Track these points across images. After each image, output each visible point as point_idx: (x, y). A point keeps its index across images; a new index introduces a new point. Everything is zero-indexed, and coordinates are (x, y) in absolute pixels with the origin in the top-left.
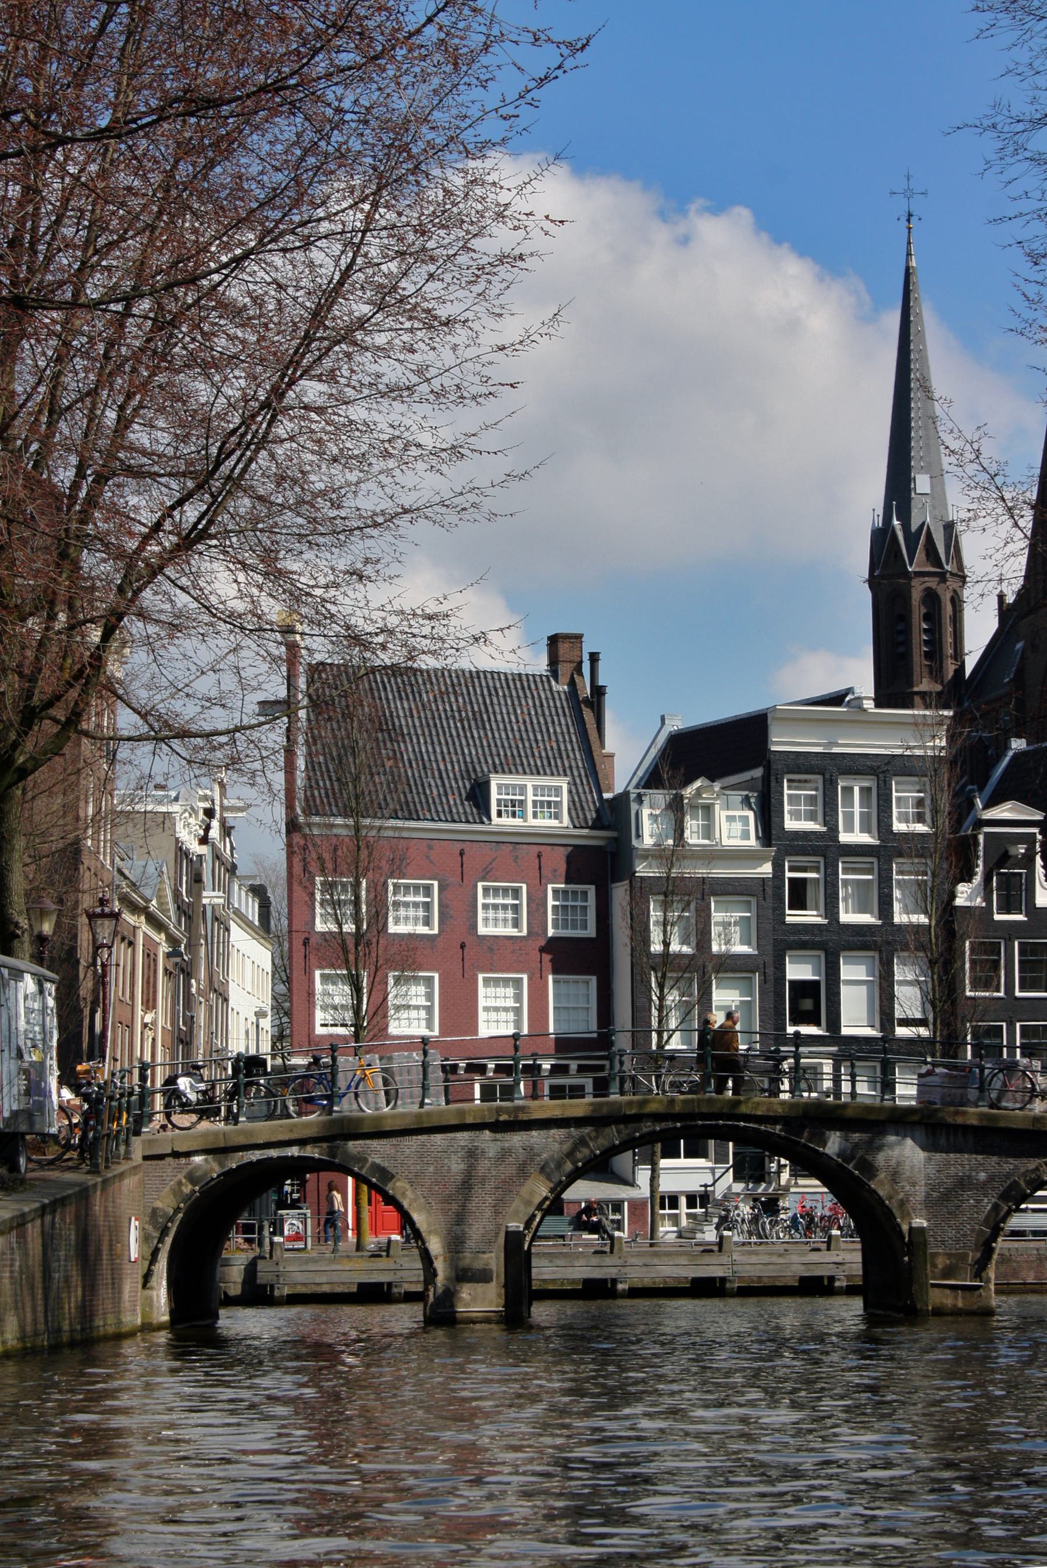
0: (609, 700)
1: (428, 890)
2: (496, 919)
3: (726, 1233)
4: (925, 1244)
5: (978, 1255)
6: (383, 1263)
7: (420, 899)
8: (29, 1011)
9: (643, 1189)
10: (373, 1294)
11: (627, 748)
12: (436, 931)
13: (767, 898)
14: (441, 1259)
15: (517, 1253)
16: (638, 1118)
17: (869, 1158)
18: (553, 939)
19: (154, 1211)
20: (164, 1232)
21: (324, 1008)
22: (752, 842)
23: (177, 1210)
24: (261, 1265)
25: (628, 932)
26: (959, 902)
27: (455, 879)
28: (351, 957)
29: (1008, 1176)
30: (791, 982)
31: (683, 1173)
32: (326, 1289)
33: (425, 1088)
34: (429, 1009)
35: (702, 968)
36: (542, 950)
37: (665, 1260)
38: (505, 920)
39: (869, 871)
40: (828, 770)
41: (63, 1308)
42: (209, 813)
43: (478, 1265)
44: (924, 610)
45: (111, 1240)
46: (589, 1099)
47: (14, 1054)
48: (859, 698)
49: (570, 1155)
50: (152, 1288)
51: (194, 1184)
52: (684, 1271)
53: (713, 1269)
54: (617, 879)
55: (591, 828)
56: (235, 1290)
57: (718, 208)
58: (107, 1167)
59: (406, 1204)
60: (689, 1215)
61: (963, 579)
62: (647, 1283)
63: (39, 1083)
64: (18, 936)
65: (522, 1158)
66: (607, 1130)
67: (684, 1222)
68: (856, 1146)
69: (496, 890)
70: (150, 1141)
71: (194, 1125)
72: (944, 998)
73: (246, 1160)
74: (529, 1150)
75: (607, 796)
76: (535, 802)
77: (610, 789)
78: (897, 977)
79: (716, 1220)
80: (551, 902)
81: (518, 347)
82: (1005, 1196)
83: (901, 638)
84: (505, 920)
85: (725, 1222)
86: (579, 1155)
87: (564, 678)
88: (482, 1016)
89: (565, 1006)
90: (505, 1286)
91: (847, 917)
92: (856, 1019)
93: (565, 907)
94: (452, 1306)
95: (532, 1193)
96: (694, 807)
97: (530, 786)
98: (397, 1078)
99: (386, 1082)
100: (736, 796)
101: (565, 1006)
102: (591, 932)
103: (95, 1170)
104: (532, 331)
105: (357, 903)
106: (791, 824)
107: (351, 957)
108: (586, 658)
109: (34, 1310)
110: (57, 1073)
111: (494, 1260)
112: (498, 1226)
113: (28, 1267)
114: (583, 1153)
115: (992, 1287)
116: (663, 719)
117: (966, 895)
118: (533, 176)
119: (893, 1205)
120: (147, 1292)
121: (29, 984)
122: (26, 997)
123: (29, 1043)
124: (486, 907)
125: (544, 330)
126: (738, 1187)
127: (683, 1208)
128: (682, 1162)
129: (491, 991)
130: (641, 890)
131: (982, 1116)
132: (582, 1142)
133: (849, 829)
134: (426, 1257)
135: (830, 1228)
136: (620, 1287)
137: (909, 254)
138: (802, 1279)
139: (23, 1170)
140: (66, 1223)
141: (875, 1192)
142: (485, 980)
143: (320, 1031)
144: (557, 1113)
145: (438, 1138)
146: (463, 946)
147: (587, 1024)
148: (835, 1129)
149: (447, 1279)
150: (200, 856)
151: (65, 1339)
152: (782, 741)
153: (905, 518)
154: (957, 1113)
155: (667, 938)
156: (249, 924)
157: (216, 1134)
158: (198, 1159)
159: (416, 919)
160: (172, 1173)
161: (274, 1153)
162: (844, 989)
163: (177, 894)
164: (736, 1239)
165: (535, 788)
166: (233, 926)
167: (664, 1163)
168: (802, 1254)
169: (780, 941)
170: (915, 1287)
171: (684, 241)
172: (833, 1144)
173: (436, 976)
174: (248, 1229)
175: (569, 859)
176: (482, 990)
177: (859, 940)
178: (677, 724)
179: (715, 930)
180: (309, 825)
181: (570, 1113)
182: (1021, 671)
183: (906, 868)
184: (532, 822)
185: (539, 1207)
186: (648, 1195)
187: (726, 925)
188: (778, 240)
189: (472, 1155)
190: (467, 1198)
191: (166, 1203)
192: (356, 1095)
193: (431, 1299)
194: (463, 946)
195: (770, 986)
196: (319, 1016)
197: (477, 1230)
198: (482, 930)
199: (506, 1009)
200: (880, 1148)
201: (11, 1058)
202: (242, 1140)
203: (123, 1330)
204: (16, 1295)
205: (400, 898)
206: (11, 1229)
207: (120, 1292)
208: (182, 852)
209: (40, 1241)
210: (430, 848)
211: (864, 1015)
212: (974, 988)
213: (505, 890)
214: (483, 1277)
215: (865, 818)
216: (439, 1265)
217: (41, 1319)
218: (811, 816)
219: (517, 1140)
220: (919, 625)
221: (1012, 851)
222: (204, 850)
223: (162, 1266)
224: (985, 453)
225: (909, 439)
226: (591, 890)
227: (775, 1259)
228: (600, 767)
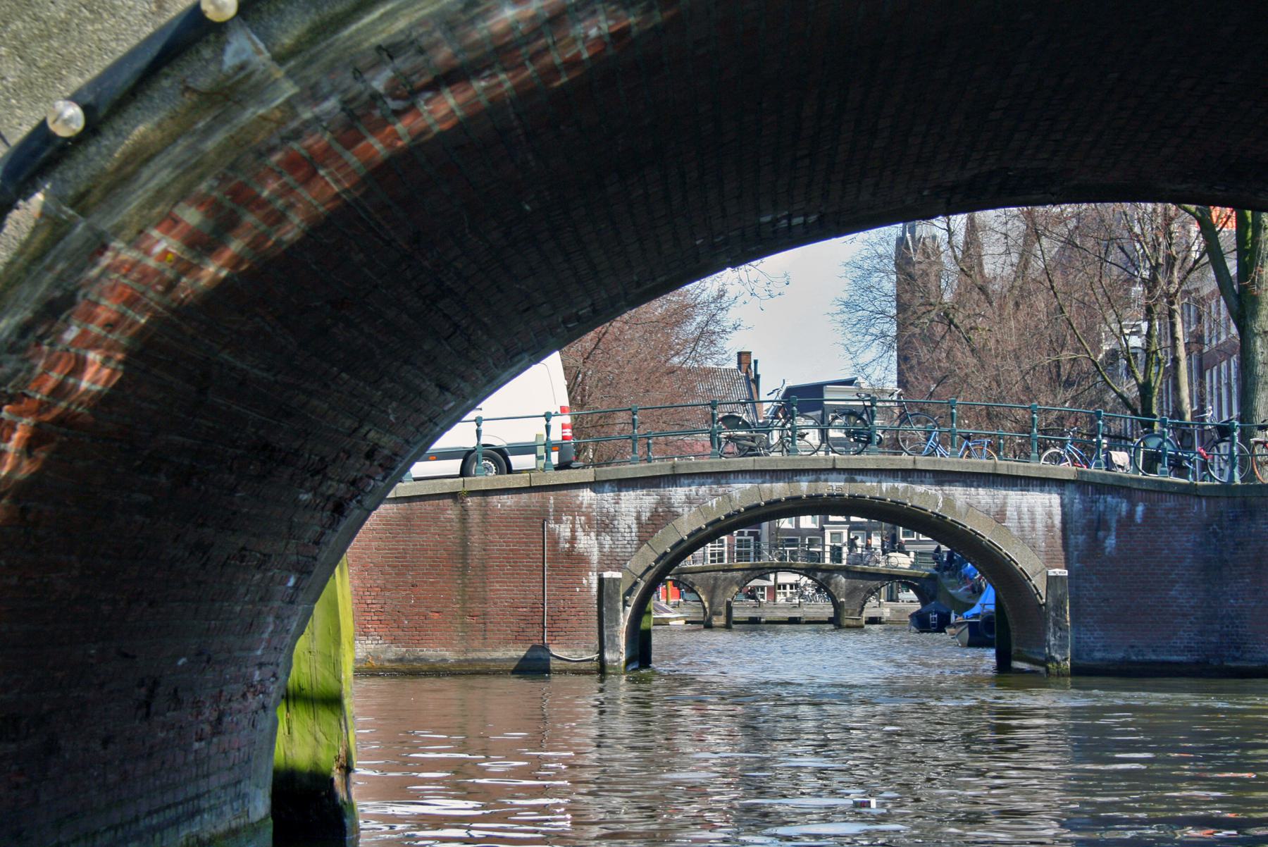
0: (761, 380)
9: (772, 583)
53: (796, 614)
111: (723, 609)
178: (790, 383)
214: (720, 614)
219: (729, 574)
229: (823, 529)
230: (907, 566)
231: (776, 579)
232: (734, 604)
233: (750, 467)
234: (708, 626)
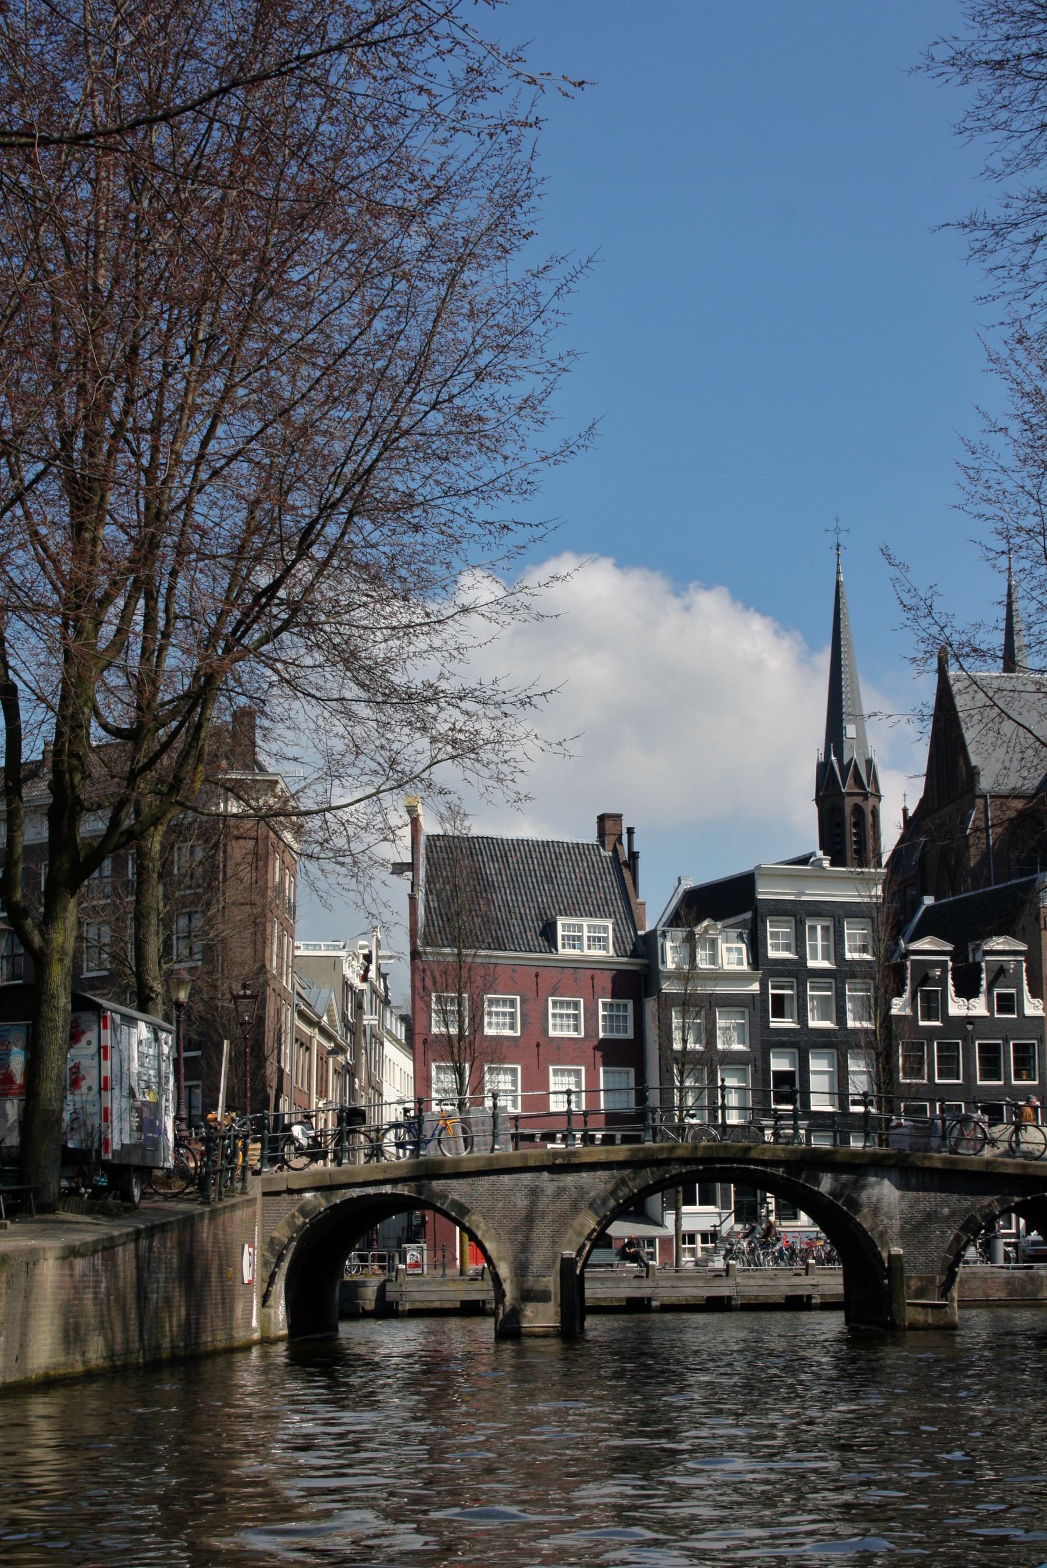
0: (641, 863)
1: (513, 1003)
2: (562, 1025)
3: (731, 1262)
4: (902, 1268)
5: (944, 1278)
7: (508, 1010)
8: (142, 1056)
9: (670, 1229)
11: (656, 899)
12: (519, 1034)
14: (509, 1281)
15: (572, 1279)
16: (667, 1162)
17: (854, 1196)
18: (603, 1040)
19: (272, 1239)
20: (280, 1258)
22: (745, 967)
23: (291, 1239)
24: (389, 1287)
25: (657, 1031)
26: (894, 1011)
27: (531, 995)
28: (456, 1050)
29: (966, 1211)
30: (775, 1072)
31: (699, 1217)
32: (437, 1305)
33: (495, 1136)
36: (595, 1048)
37: (687, 1283)
38: (568, 1026)
40: (799, 913)
41: (163, 1327)
42: (368, 958)
43: (540, 1287)
45: (221, 1265)
47: (125, 1093)
49: (613, 1193)
50: (270, 1307)
51: (305, 1217)
53: (723, 1289)
54: (648, 995)
55: (630, 957)
56: (370, 1305)
57: (708, 588)
58: (220, 1199)
59: (479, 1234)
60: (703, 1249)
61: (879, 797)
62: (674, 1300)
63: (153, 1122)
64: (152, 999)
65: (574, 1195)
66: (643, 1172)
67: (699, 1254)
68: (844, 1186)
69: (562, 1003)
70: (269, 1180)
71: (306, 1166)
73: (348, 1196)
74: (580, 1188)
75: (640, 933)
76: (589, 938)
77: (643, 928)
78: (850, 1069)
79: (723, 1252)
81: (558, 457)
82: (964, 1228)
83: (838, 839)
84: (568, 1026)
85: (729, 1254)
86: (620, 1194)
90: (561, 1305)
93: (611, 1016)
94: (518, 1322)
95: (583, 1225)
98: (474, 1129)
99: (464, 1131)
100: (733, 933)
102: (630, 1035)
103: (206, 1202)
104: (571, 442)
105: (460, 1013)
106: (772, 954)
107: (456, 1050)
108: (624, 831)
109: (126, 1329)
110: (172, 1114)
111: (551, 1282)
112: (555, 1254)
113: (117, 1289)
114: (624, 1192)
115: (956, 1305)
116: (679, 880)
117: (899, 1006)
118: (569, 278)
119: (874, 1235)
120: (266, 1310)
121: (142, 1031)
122: (140, 1043)
123: (143, 1085)
124: (554, 1015)
125: (581, 442)
126: (738, 1228)
127: (699, 1243)
128: (697, 1208)
129: (559, 1079)
130: (666, 1003)
131: (945, 1160)
132: (623, 1182)
133: (814, 957)
135: (807, 1258)
136: (654, 1303)
137: (838, 572)
138: (788, 1297)
139: (137, 1199)
140: (167, 1250)
141: (860, 1224)
144: (602, 1158)
145: (506, 1179)
146: (538, 1045)
147: (627, 1103)
148: (826, 1171)
149: (514, 1299)
150: (362, 991)
151: (164, 1356)
152: (765, 892)
153: (839, 755)
154: (924, 1158)
157: (323, 1174)
158: (308, 1195)
159: (504, 1024)
160: (288, 1207)
161: (371, 1190)
162: (812, 1078)
163: (344, 1016)
164: (738, 1266)
165: (589, 926)
166: (387, 1044)
167: (685, 1209)
169: (767, 1042)
170: (895, 1306)
171: (687, 609)
172: (826, 1184)
173: (519, 1067)
174: (381, 1258)
175: (615, 980)
176: (552, 1078)
177: (822, 1040)
178: (688, 884)
180: (426, 953)
181: (612, 1158)
182: (923, 857)
183: (858, 986)
184: (587, 952)
185: (588, 1238)
186: (673, 1233)
188: (747, 607)
189: (534, 1193)
190: (530, 1230)
191: (282, 1233)
192: (439, 1142)
193: (501, 1316)
194: (538, 1045)
195: (759, 1075)
197: (539, 1256)
198: (552, 1033)
200: (863, 1188)
201: (122, 1096)
202: (345, 1180)
203: (236, 1344)
204: (102, 1316)
205: (494, 1009)
206: (95, 1252)
207: (232, 1310)
208: (347, 986)
209: (134, 1264)
210: (514, 971)
212: (905, 1076)
213: (568, 1003)
214: (543, 1297)
216: (507, 1287)
217: (134, 1335)
218: (787, 948)
219: (570, 1180)
220: (851, 830)
221: (931, 973)
222: (364, 986)
223: (280, 1287)
224: (936, 609)
225: (841, 700)
226: (630, 1003)
227: (768, 1282)
228: (636, 912)
231: (678, 1221)
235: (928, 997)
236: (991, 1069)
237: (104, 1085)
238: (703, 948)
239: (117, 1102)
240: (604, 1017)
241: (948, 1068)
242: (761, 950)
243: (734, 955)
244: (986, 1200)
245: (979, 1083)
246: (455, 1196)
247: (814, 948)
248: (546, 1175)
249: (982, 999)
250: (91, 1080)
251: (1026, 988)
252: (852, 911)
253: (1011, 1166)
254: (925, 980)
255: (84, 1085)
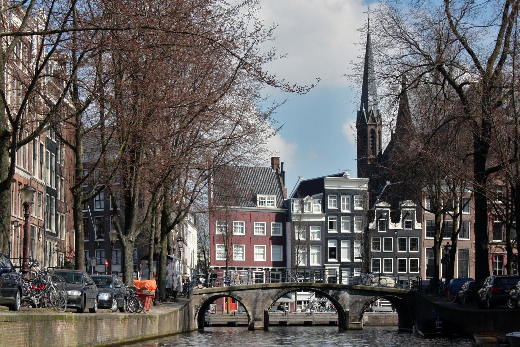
0: (286, 174)
1: (242, 224)
6: (233, 317)
10: (231, 324)
11: (291, 186)
13: (324, 226)
16: (291, 287)
18: (272, 237)
21: (218, 253)
22: (320, 212)
27: (248, 221)
31: (303, 296)
32: (220, 323)
34: (243, 254)
35: (308, 244)
36: (270, 239)
37: (298, 317)
39: (348, 220)
40: (338, 194)
43: (259, 318)
44: (371, 135)
46: (281, 283)
48: (347, 175)
49: (277, 295)
52: (302, 320)
53: (309, 319)
62: (294, 323)
67: (303, 308)
68: (335, 293)
69: (259, 224)
72: (366, 253)
74: (269, 294)
75: (285, 200)
77: (286, 198)
80: (272, 227)
82: (365, 304)
85: (312, 308)
87: (275, 169)
88: (255, 256)
89: (275, 254)
91: (343, 231)
92: (345, 258)
96: (306, 203)
97: (267, 197)
99: (240, 279)
101: (275, 254)
102: (281, 235)
106: (330, 207)
108: (280, 163)
111: (262, 316)
117: (372, 226)
119: (342, 306)
124: (256, 228)
126: (316, 299)
127: (303, 304)
129: (257, 249)
130: (293, 224)
132: (280, 292)
134: (248, 316)
138: (330, 322)
142: (256, 247)
143: (217, 259)
145: (251, 291)
152: (328, 186)
153: (366, 108)
155: (299, 237)
156: (191, 224)
158: (204, 295)
160: (199, 298)
162: (342, 249)
167: (298, 293)
168: (330, 316)
169: (327, 237)
172: (331, 293)
177: (345, 237)
178: (303, 179)
179: (311, 235)
181: (277, 286)
184: (267, 206)
187: (313, 233)
189: (257, 294)
190: (256, 304)
191: (198, 304)
195: (324, 249)
196: (217, 256)
197: (258, 310)
198: (255, 234)
199: (261, 254)
200: (340, 294)
202: (212, 291)
211: (348, 256)
213: (261, 224)
214: (260, 320)
215: (348, 207)
216: (251, 317)
218: (335, 205)
219: (266, 291)
220: (370, 139)
223: (197, 317)
226: (281, 224)
228: (284, 192)
229: (324, 267)
230: (393, 285)
231: (296, 297)
232: (270, 313)
233: (275, 286)
234: (252, 328)
235: (382, 223)
236: (403, 247)
237: (173, 275)
238: (306, 206)
239: (175, 278)
240: (273, 229)
241: (388, 246)
242: (326, 206)
243: (317, 208)
244: (371, 297)
245: (398, 252)
246: (238, 295)
247: (344, 205)
248: (260, 290)
249: (400, 223)
250: (170, 274)
251: (416, 219)
252: (356, 192)
253: (378, 289)
254: (381, 216)
255: (169, 275)
